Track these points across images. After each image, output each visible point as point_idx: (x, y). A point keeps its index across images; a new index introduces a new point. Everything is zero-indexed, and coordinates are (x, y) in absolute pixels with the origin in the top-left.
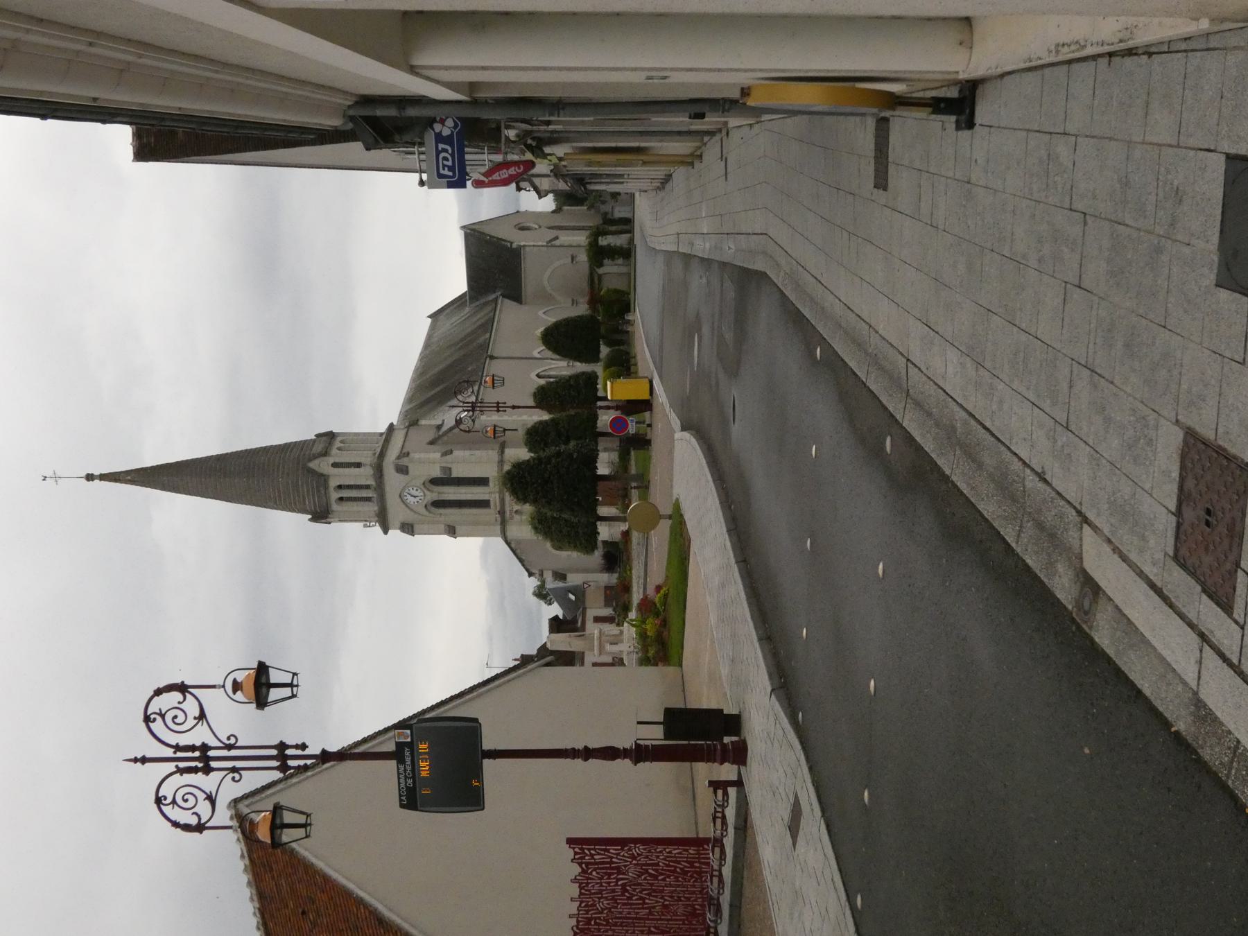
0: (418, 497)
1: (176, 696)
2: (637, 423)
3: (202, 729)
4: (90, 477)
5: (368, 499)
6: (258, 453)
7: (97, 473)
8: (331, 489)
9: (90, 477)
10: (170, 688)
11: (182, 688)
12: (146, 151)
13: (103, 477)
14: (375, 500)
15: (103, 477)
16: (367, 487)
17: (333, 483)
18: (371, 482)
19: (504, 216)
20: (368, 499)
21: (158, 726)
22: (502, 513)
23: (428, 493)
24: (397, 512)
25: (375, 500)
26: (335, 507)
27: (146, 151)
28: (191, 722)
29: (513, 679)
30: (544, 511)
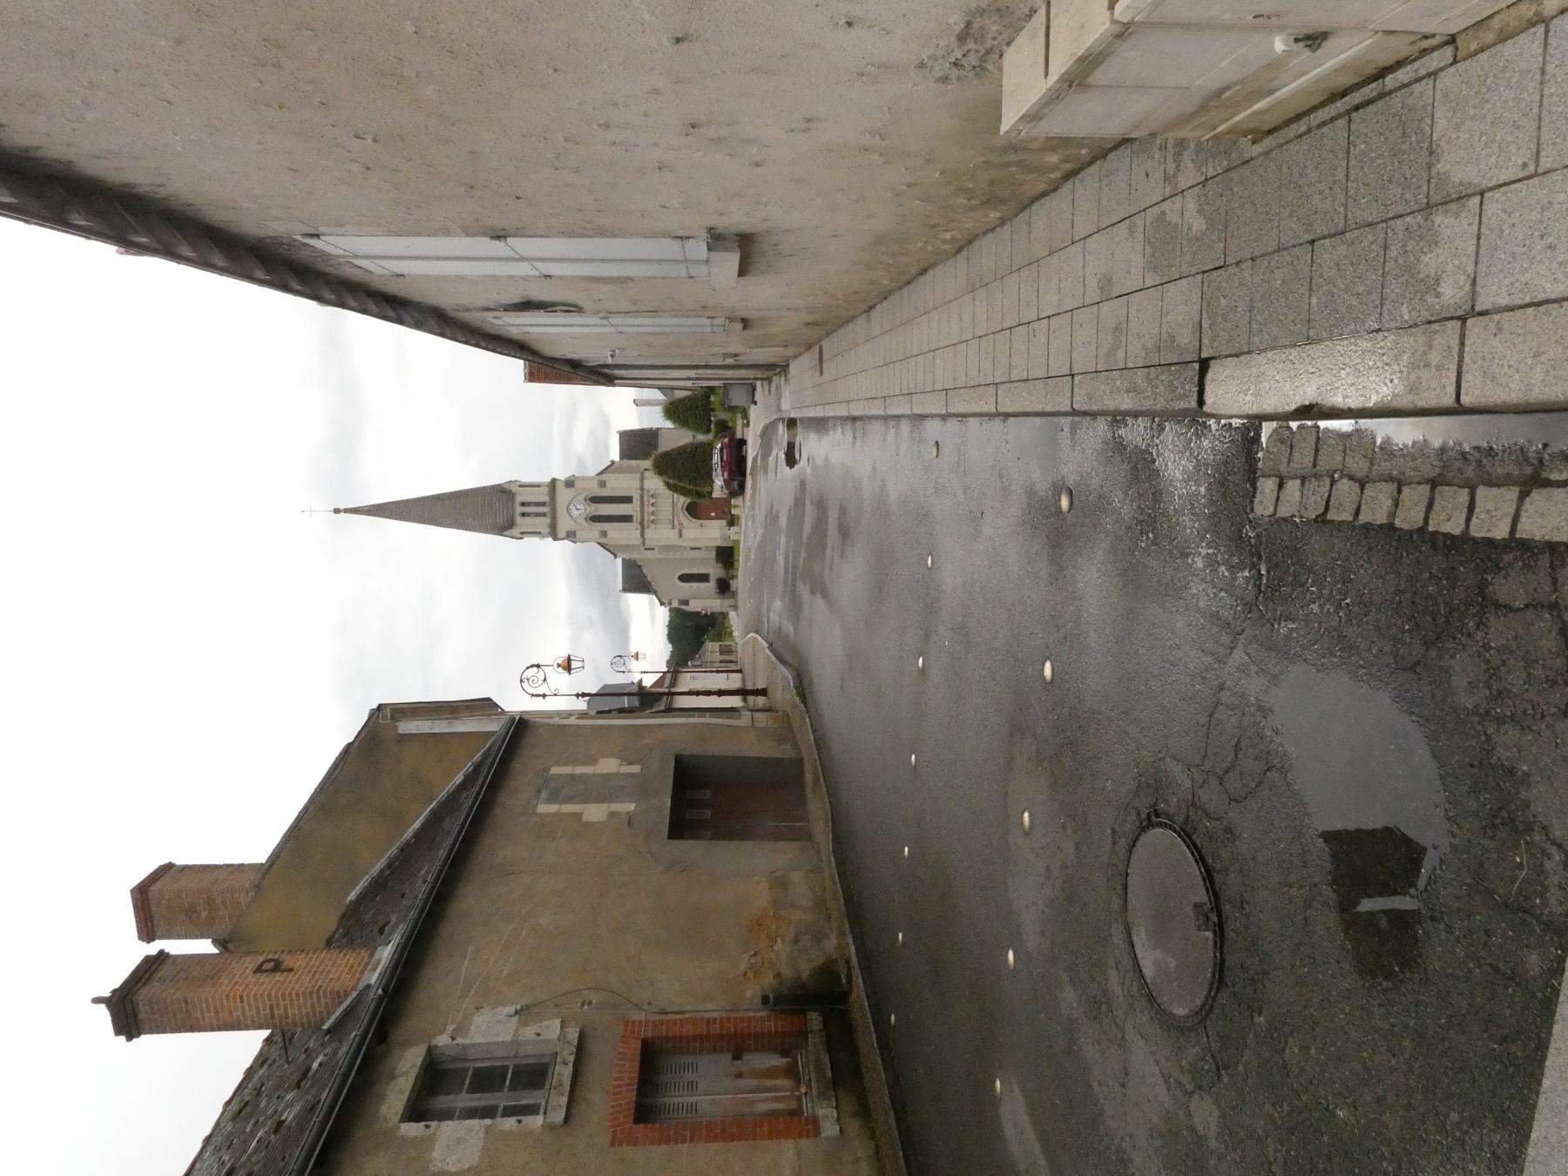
0: (581, 509)
1: (535, 669)
2: (640, 1022)
3: (545, 685)
4: (337, 511)
5: (544, 515)
6: (1524, 1101)
7: (342, 508)
8: (517, 505)
9: (337, 511)
10: (532, 666)
11: (538, 666)
12: (532, 376)
13: (346, 511)
14: (548, 514)
15: (346, 511)
16: (543, 504)
17: (519, 499)
18: (546, 499)
19: (655, 278)
20: (544, 515)
21: (525, 685)
22: (642, 524)
23: (588, 507)
24: (564, 525)
25: (548, 514)
26: (519, 520)
27: (532, 376)
28: (540, 682)
29: (1314, 109)
30: (797, 877)
